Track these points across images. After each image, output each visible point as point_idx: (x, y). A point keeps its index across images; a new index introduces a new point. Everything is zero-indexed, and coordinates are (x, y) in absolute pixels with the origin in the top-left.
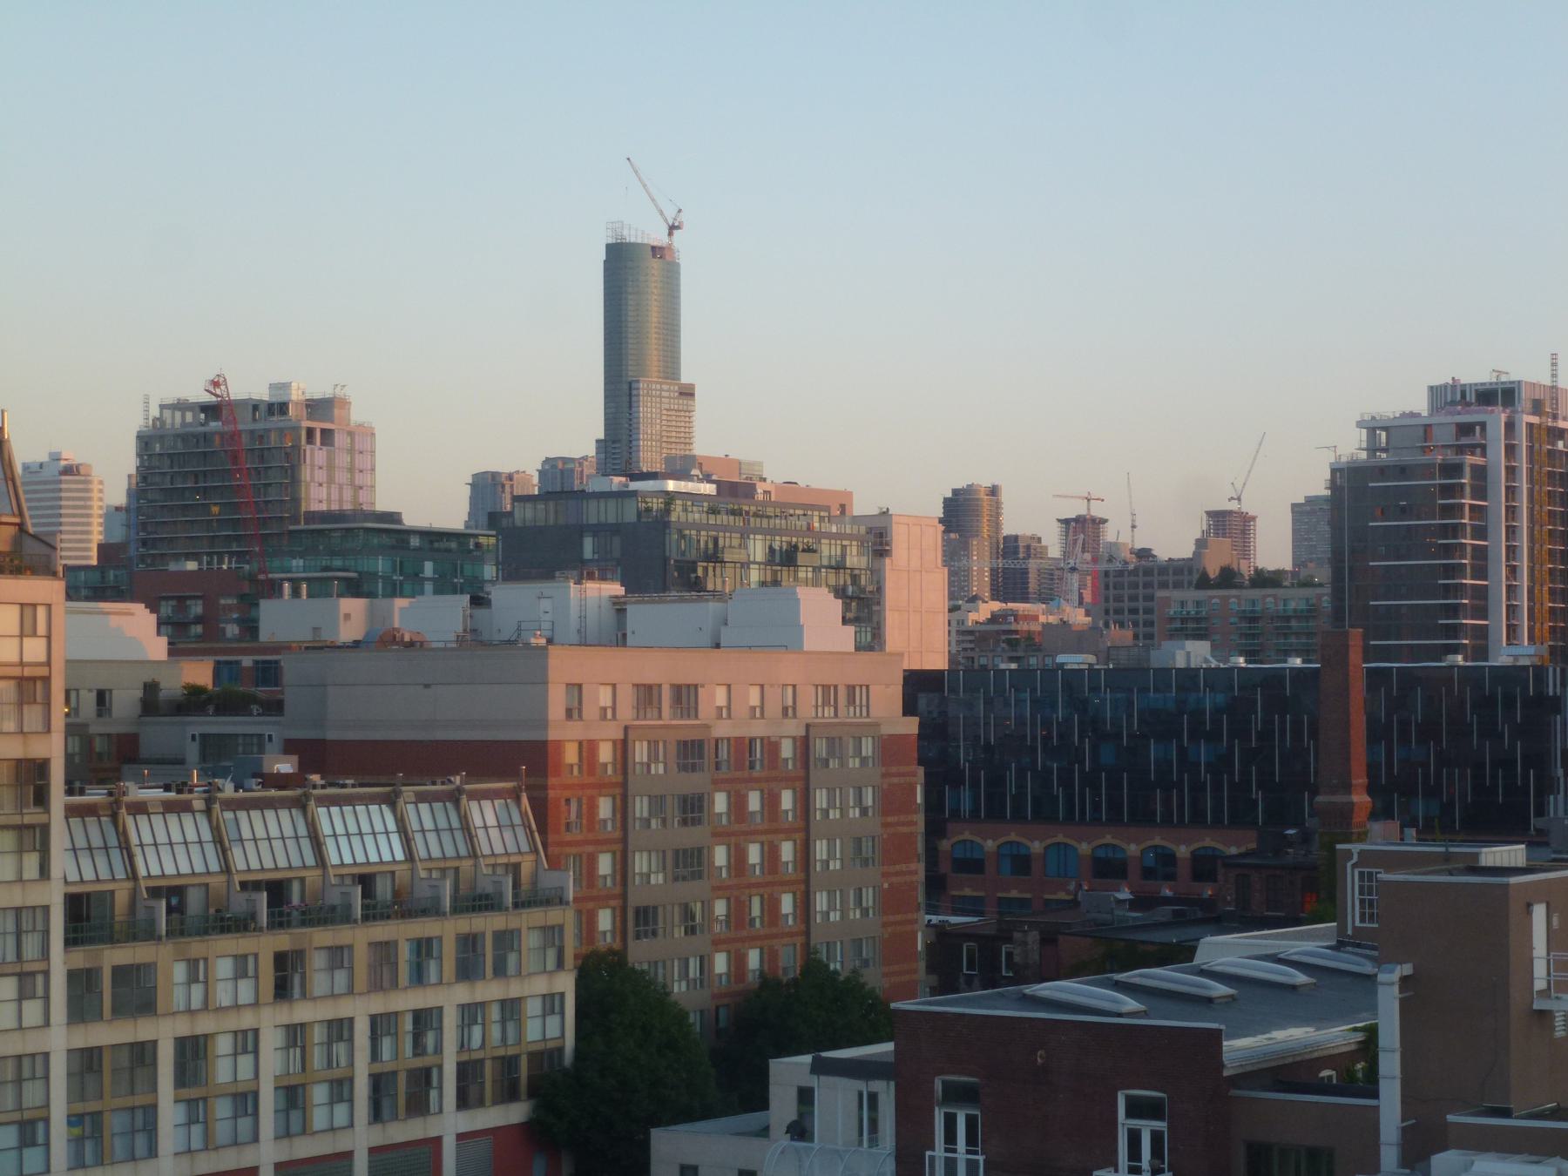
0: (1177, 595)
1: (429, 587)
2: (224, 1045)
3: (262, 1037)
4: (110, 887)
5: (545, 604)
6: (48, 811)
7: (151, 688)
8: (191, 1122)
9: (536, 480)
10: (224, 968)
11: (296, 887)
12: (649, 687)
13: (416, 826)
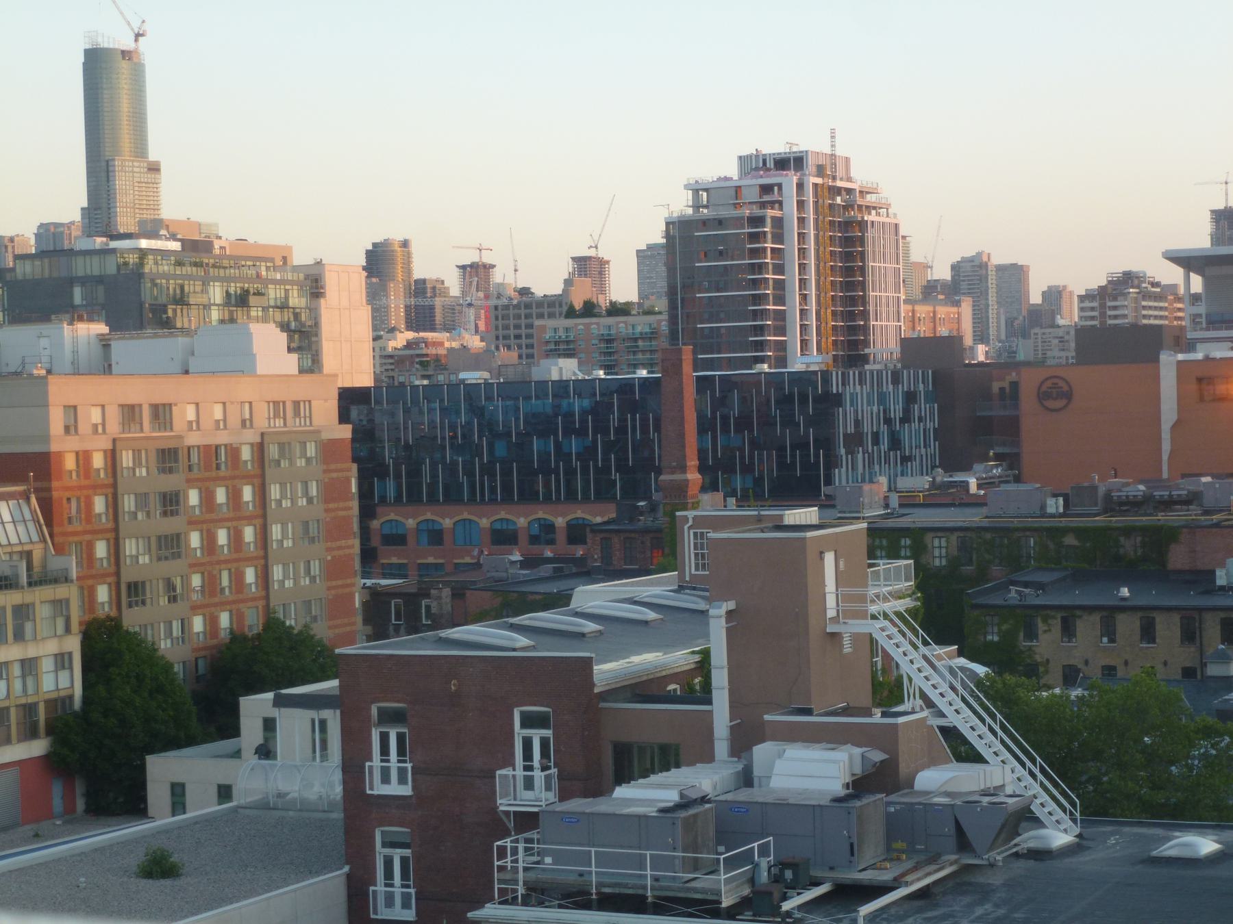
1: (413, 301)
5: (44, 342)
9: (33, 242)
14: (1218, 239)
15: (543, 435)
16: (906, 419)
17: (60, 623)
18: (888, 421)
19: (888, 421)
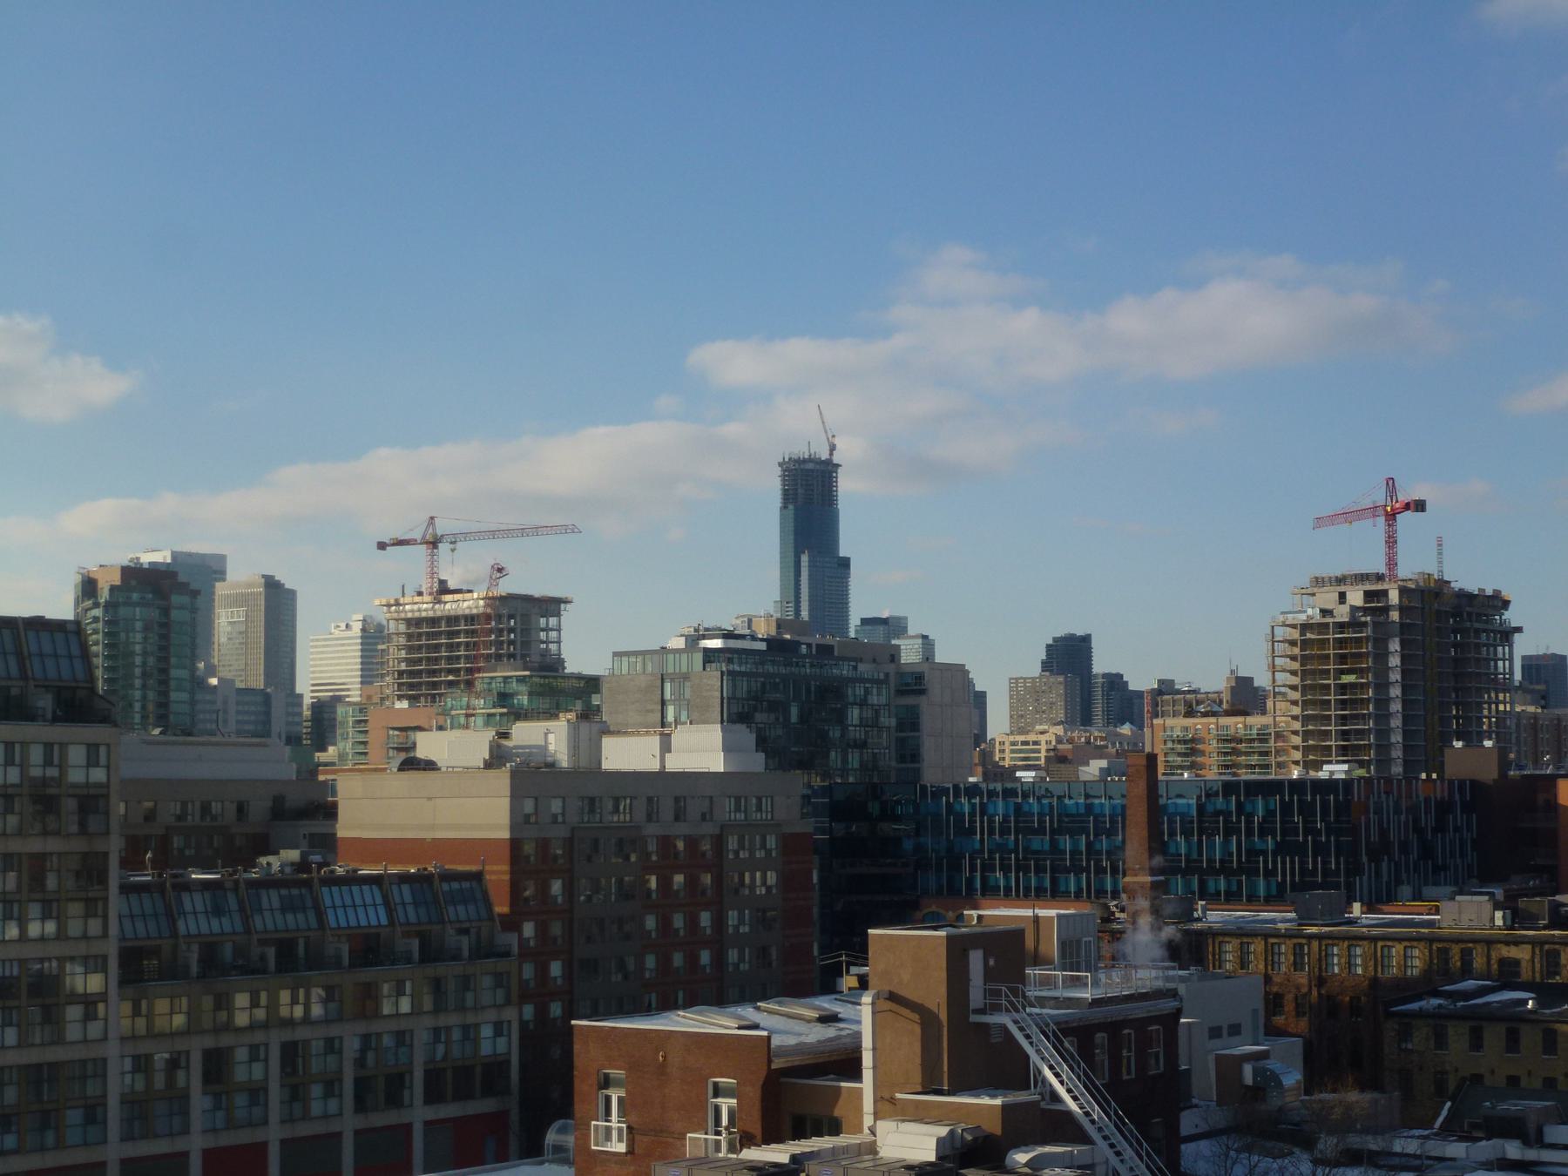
0: (1170, 722)
2: (242, 1054)
3: (109, 1066)
4: (158, 942)
6: (107, 889)
7: (278, 801)
8: (217, 1107)
10: (487, 981)
11: (301, 941)
12: (592, 800)
13: (398, 900)
14: (1538, 668)
15: (1073, 833)
16: (1440, 828)
17: (500, 993)
18: (1419, 830)
19: (1419, 830)
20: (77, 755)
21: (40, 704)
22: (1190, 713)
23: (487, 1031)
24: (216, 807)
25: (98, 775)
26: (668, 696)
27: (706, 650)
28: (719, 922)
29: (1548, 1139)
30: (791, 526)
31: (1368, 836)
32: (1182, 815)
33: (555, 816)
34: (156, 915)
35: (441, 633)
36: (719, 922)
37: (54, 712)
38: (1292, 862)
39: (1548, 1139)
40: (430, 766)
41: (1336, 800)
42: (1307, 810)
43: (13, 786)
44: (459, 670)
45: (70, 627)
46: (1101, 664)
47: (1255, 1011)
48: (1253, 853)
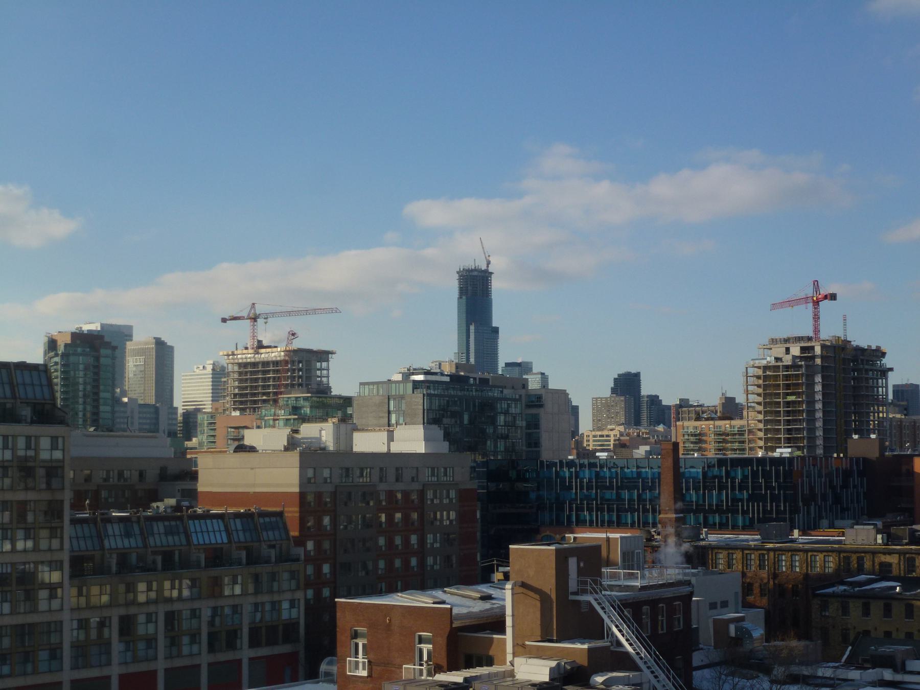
0: (686, 423)
2: (142, 619)
3: (64, 625)
4: (93, 553)
6: (63, 522)
7: (163, 470)
8: (127, 650)
10: (286, 576)
11: (177, 552)
12: (347, 469)
13: (233, 528)
15: (630, 489)
16: (845, 486)
17: (294, 583)
18: (832, 487)
19: (832, 487)
20: (45, 443)
21: (24, 413)
22: (698, 418)
23: (285, 605)
24: (127, 474)
25: (58, 455)
26: (392, 408)
27: (414, 382)
28: (422, 541)
29: (909, 668)
30: (464, 309)
31: (803, 491)
32: (694, 478)
33: (326, 479)
34: (91, 537)
35: (258, 371)
36: (422, 541)
37: (32, 418)
38: (758, 506)
39: (909, 668)
40: (252, 449)
41: (784, 469)
42: (767, 475)
43: (7, 461)
44: (269, 393)
45: (41, 368)
46: (646, 390)
47: (736, 593)
48: (735, 500)
